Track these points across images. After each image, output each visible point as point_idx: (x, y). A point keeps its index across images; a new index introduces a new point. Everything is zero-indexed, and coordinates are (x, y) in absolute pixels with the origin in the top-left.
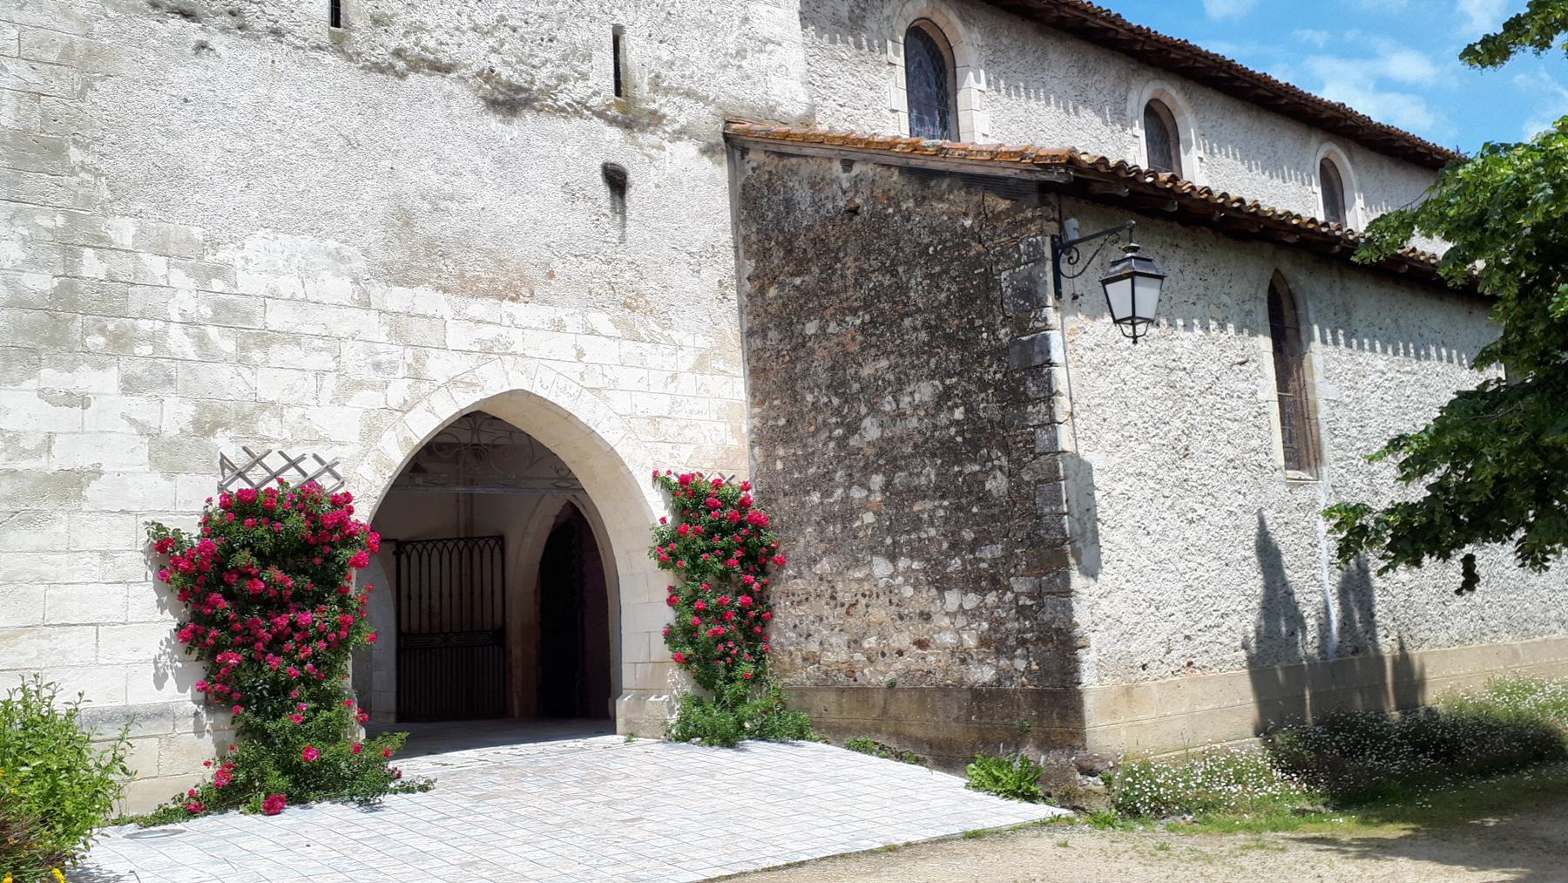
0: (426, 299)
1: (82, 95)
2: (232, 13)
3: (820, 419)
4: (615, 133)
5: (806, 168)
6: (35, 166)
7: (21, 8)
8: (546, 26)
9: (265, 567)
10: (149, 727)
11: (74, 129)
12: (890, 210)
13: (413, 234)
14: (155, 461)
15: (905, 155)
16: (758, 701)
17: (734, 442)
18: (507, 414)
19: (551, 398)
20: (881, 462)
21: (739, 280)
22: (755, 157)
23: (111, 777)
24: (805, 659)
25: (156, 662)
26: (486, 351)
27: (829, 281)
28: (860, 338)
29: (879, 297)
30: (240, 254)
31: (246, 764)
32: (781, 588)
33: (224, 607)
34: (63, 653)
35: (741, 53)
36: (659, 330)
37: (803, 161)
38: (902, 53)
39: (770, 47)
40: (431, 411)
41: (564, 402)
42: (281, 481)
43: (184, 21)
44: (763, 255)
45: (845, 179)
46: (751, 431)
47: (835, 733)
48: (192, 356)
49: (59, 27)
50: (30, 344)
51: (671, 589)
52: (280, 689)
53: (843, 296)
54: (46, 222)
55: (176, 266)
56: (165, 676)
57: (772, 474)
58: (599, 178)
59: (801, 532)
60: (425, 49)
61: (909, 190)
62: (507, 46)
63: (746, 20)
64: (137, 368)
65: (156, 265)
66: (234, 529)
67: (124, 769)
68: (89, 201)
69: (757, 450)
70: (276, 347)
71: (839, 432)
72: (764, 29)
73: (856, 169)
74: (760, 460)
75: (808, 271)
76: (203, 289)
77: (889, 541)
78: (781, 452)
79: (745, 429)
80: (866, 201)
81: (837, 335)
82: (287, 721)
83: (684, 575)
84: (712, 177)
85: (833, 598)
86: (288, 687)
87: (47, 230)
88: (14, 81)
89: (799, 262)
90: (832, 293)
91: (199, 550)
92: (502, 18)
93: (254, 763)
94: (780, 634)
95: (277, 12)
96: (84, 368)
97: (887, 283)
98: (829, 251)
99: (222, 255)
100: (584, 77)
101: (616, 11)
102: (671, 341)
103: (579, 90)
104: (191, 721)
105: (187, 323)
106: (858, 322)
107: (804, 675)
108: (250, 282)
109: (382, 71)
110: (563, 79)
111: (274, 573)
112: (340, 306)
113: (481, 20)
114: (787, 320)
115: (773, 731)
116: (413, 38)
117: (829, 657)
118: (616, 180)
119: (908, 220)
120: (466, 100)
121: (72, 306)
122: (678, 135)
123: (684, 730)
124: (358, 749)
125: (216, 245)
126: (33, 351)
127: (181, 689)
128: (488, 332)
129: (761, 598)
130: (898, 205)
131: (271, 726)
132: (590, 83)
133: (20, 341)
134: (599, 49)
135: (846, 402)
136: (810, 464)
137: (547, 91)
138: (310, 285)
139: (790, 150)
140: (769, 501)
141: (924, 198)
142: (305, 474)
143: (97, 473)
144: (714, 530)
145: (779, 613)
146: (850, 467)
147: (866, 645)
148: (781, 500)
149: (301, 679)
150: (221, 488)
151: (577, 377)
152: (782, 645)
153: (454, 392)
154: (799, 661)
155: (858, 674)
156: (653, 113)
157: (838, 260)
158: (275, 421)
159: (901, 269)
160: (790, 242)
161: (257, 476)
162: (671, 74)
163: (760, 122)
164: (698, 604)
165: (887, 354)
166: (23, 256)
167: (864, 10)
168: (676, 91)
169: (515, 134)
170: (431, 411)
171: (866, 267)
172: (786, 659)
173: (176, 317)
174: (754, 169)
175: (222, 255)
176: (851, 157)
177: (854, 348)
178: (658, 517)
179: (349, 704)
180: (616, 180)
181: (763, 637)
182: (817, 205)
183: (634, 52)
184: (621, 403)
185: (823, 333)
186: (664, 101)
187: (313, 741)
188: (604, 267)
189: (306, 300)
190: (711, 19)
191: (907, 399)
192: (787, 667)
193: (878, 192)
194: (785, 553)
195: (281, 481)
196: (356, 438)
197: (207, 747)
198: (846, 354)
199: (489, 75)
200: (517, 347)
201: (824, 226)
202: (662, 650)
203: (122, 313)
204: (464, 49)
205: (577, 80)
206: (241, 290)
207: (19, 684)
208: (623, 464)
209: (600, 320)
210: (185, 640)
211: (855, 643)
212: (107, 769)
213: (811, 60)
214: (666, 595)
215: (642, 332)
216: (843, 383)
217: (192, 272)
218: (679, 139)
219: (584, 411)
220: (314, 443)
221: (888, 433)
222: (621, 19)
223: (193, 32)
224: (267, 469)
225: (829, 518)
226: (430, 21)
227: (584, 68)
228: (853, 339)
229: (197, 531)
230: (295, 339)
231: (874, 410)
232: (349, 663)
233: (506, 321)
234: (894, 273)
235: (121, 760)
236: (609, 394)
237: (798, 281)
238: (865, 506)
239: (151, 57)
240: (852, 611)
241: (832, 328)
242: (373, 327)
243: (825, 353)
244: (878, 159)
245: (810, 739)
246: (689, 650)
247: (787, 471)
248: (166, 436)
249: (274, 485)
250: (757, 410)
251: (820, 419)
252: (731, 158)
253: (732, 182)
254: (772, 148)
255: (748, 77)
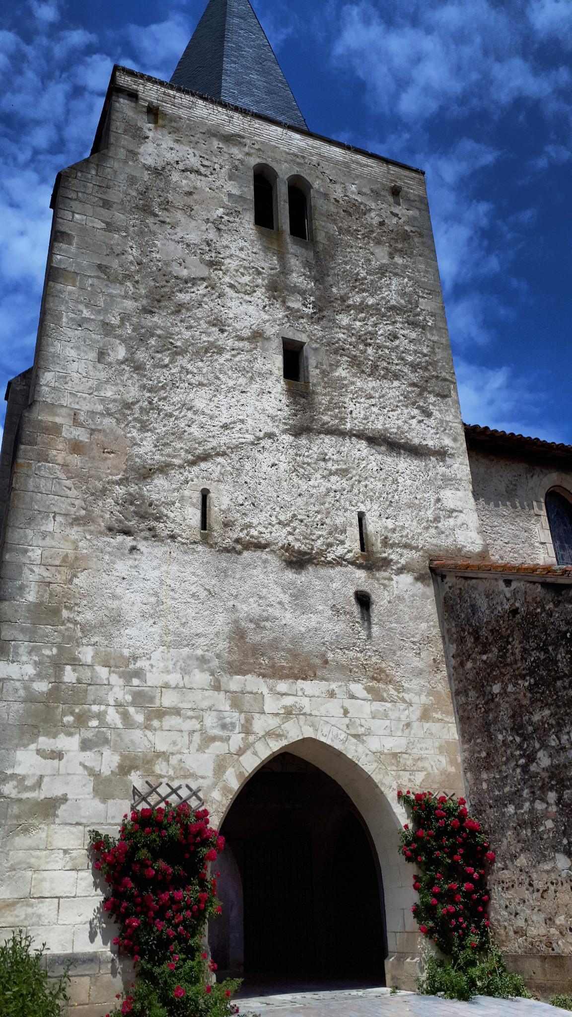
0: (253, 683)
1: (70, 581)
2: (150, 529)
3: (509, 752)
4: (361, 574)
5: (482, 586)
6: (45, 622)
7: (44, 539)
8: (319, 516)
9: (155, 859)
10: (80, 970)
11: (65, 600)
12: (539, 610)
13: (245, 643)
14: (96, 791)
15: (543, 576)
16: (485, 964)
17: (452, 769)
18: (301, 753)
19: (328, 742)
20: (553, 783)
21: (447, 658)
22: (450, 580)
23: (57, 1002)
24: (516, 933)
25: (91, 923)
26: (288, 713)
27: (504, 656)
28: (529, 695)
29: (538, 667)
30: (149, 662)
31: (142, 998)
32: (494, 877)
33: (130, 885)
34: (39, 916)
35: (437, 519)
36: (396, 693)
37: (479, 581)
38: (544, 508)
39: (455, 514)
40: (255, 753)
41: (337, 746)
42: (167, 803)
43: (125, 537)
44: (461, 641)
45: (507, 591)
46: (464, 761)
47: (542, 991)
48: (121, 726)
49: (62, 546)
50: (34, 723)
51: (415, 877)
52: (164, 943)
53: (515, 667)
54: (47, 652)
55: (114, 672)
56: (96, 933)
57: (480, 792)
58: (353, 599)
59: (504, 835)
60: (252, 537)
61: (549, 597)
62: (298, 530)
63: (438, 500)
64: (89, 734)
65: (103, 672)
66: (139, 834)
67: (65, 996)
68: (70, 639)
69: (469, 775)
70: (167, 717)
71: (522, 761)
72: (450, 504)
73: (514, 585)
74: (472, 782)
75: (491, 651)
76: (128, 683)
77: (565, 841)
78: (485, 776)
79: (459, 760)
80: (522, 605)
81: (514, 693)
82: (166, 967)
83: (423, 867)
84: (424, 594)
85: (531, 885)
86: (169, 942)
87: (48, 656)
88: (37, 577)
89: (484, 645)
90: (508, 665)
91: (119, 848)
92: (294, 516)
93: (146, 997)
94: (497, 913)
95: (173, 526)
96: (62, 736)
97: (542, 657)
98: (502, 637)
99: (139, 664)
100: (342, 542)
101: (359, 504)
102: (404, 700)
103: (340, 551)
104: (109, 966)
105: (118, 705)
106: (527, 684)
107: (515, 945)
108: (153, 679)
109: (228, 551)
110: (330, 545)
111: (161, 864)
112: (203, 689)
113: (282, 518)
114: (481, 686)
115: (497, 989)
116: (245, 532)
117: (533, 931)
118: (364, 600)
119: (551, 616)
120: (275, 562)
121: (57, 700)
122: (400, 571)
123: (432, 985)
124: (209, 989)
125: (135, 658)
126: (35, 727)
127: (105, 943)
128: (288, 701)
129: (481, 885)
130: (543, 607)
131: (157, 970)
132: (346, 546)
133: (30, 721)
134: (351, 526)
135: (525, 740)
136: (505, 785)
137: (321, 553)
138: (186, 678)
139: (471, 575)
140: (480, 812)
141: (559, 602)
142: (181, 798)
143: (64, 799)
144: (441, 833)
145: (494, 895)
146: (532, 787)
147: (558, 922)
148: (488, 811)
149: (175, 938)
150: (133, 808)
151: (345, 728)
152: (498, 921)
153: (269, 741)
154: (511, 933)
155: (554, 945)
156: (385, 559)
157: (508, 643)
158: (164, 763)
159: (550, 648)
160: (477, 632)
161: (153, 799)
162: (394, 535)
163: (453, 558)
164: (436, 889)
165: (548, 705)
166: (34, 672)
167: (515, 485)
168: (398, 545)
169: (303, 579)
170: (255, 753)
171: (528, 647)
172: (502, 932)
173: (112, 703)
174: (450, 588)
175: (139, 664)
176: (510, 577)
177: (526, 702)
178: (403, 824)
179: (205, 956)
180: (364, 600)
181: (485, 914)
182: (492, 608)
183: (372, 526)
184: (374, 744)
185: (504, 693)
186: (391, 551)
187: (182, 983)
188: (359, 655)
189: (184, 687)
190: (417, 502)
191: (566, 737)
192: (504, 938)
193: (529, 599)
194: (494, 851)
195: (167, 803)
196: (210, 774)
197: (118, 983)
198: (521, 706)
199: (288, 548)
200: (307, 710)
201: (497, 621)
202: (412, 923)
203: (83, 702)
204: (273, 534)
205: (338, 545)
206: (149, 684)
207: (11, 937)
208: (377, 787)
209: (357, 688)
210: (108, 909)
211: (549, 921)
212: (56, 996)
213: (484, 518)
214: (413, 881)
215: (385, 695)
216: (522, 726)
217: (122, 675)
218: (402, 573)
219: (352, 751)
220: (185, 777)
221: (556, 762)
222: (362, 508)
223: (129, 541)
224: (159, 795)
225: (522, 824)
226: (255, 521)
227: (342, 537)
228: (525, 695)
229: (118, 836)
230: (177, 711)
231: (544, 746)
232: (206, 927)
233: (300, 693)
234: (546, 651)
235: (64, 989)
236: (365, 738)
237: (484, 657)
238: (545, 815)
239: (107, 557)
240: (545, 895)
241: (510, 688)
242: (222, 702)
243: (507, 705)
244: (527, 578)
245: (525, 996)
246: (431, 924)
247: (490, 791)
248: (103, 776)
249: (163, 805)
250: (466, 746)
251: (509, 752)
252: (435, 581)
253: (437, 595)
254: (460, 574)
255: (443, 533)
